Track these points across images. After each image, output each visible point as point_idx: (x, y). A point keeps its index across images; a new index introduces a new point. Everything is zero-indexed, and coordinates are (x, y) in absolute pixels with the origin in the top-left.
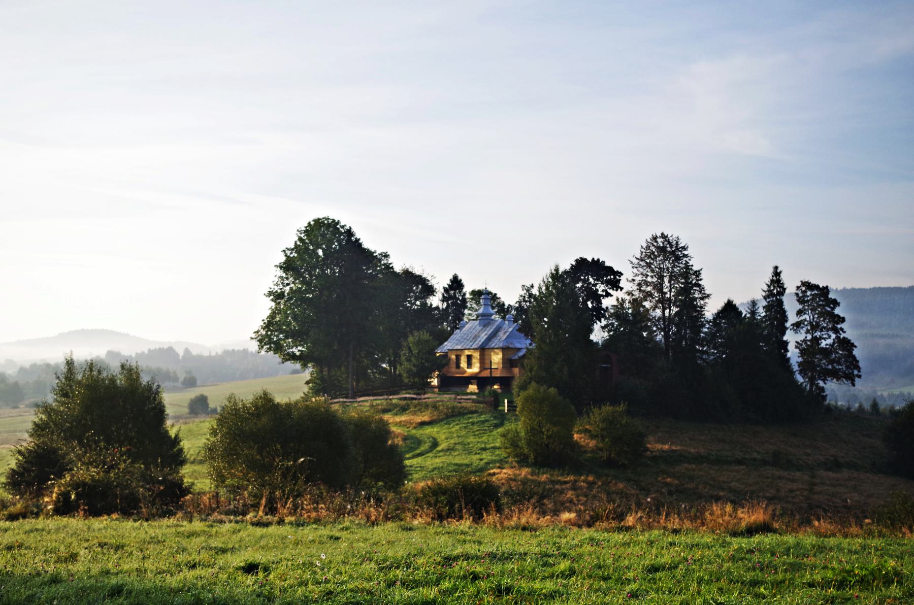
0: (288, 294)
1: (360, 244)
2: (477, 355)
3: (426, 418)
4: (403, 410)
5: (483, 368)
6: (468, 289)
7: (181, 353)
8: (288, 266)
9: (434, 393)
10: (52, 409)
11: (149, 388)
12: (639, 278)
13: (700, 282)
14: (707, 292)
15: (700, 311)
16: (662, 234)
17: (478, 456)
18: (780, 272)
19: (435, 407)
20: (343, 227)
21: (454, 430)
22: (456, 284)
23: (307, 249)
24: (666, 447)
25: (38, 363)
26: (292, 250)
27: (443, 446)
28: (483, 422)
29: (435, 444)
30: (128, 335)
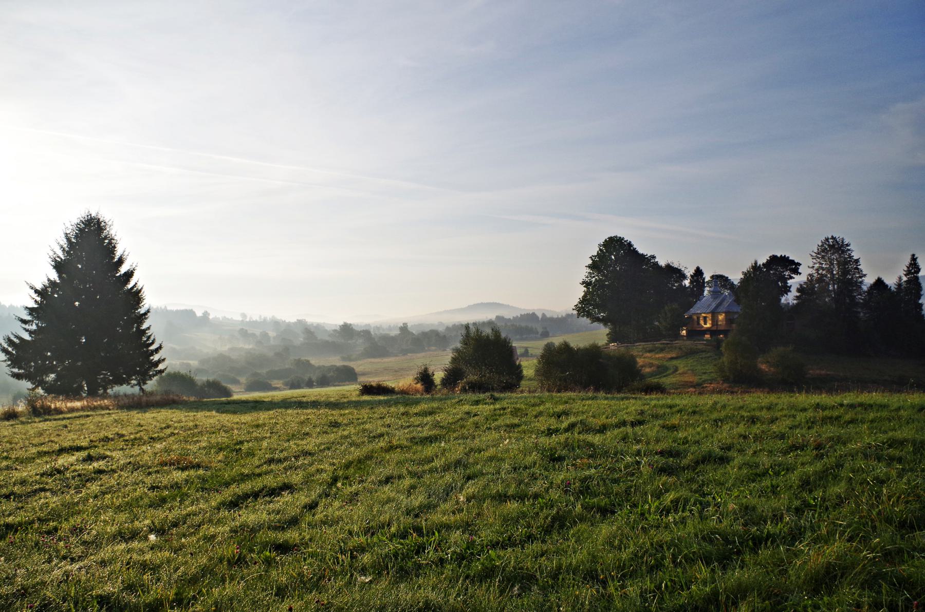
0: (594, 283)
1: (637, 252)
2: (709, 316)
3: (674, 355)
4: (662, 350)
5: (713, 324)
6: (707, 277)
7: (540, 316)
8: (594, 266)
9: (683, 340)
10: (460, 351)
11: (505, 339)
12: (817, 265)
13: (859, 267)
14: (864, 273)
15: (858, 285)
16: (832, 236)
17: (699, 377)
18: (917, 258)
19: (680, 348)
20: (626, 241)
21: (689, 362)
22: (699, 272)
23: (604, 255)
24: (823, 372)
25: (457, 324)
26: (596, 256)
27: (680, 371)
28: (709, 357)
29: (676, 369)
30: (508, 306)
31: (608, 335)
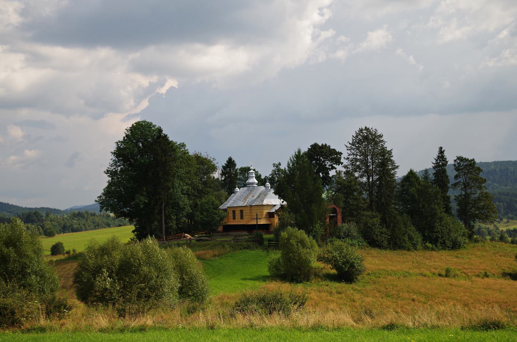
14: (397, 165)
16: (366, 128)
18: (444, 151)
31: (133, 232)
